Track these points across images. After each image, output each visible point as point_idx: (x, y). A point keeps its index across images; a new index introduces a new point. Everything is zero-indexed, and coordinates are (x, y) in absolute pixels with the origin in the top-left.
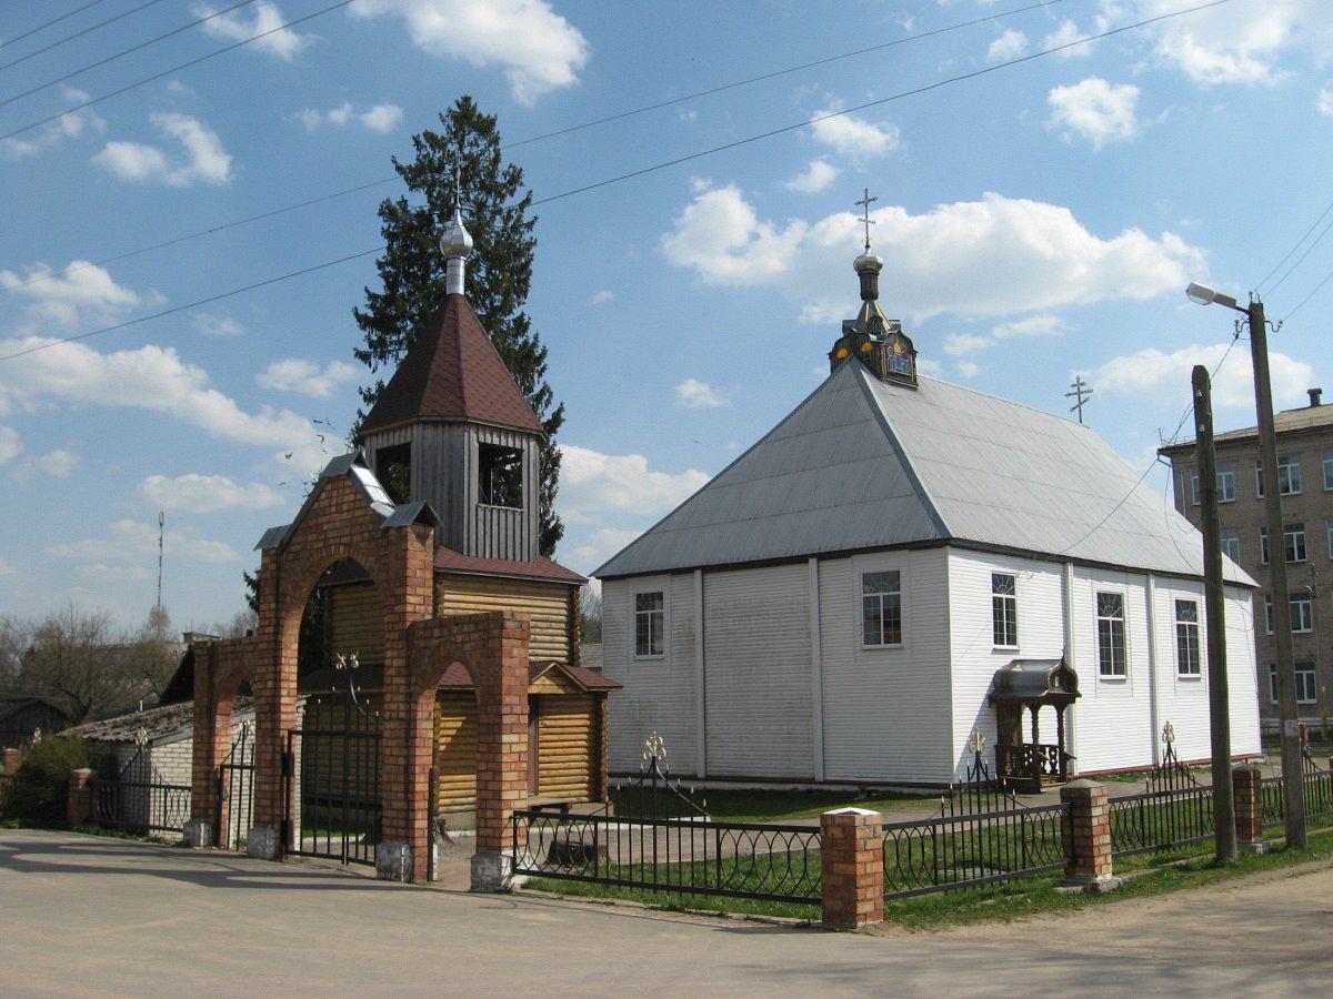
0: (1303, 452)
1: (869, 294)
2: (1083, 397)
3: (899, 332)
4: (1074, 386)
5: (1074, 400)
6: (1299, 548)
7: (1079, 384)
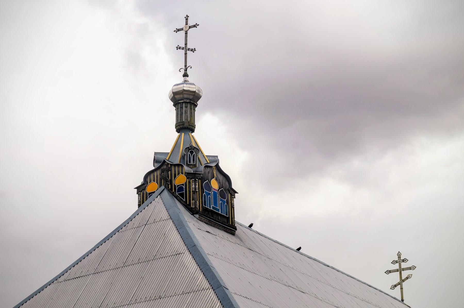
2: (405, 274)
3: (217, 167)
4: (394, 262)
7: (400, 260)
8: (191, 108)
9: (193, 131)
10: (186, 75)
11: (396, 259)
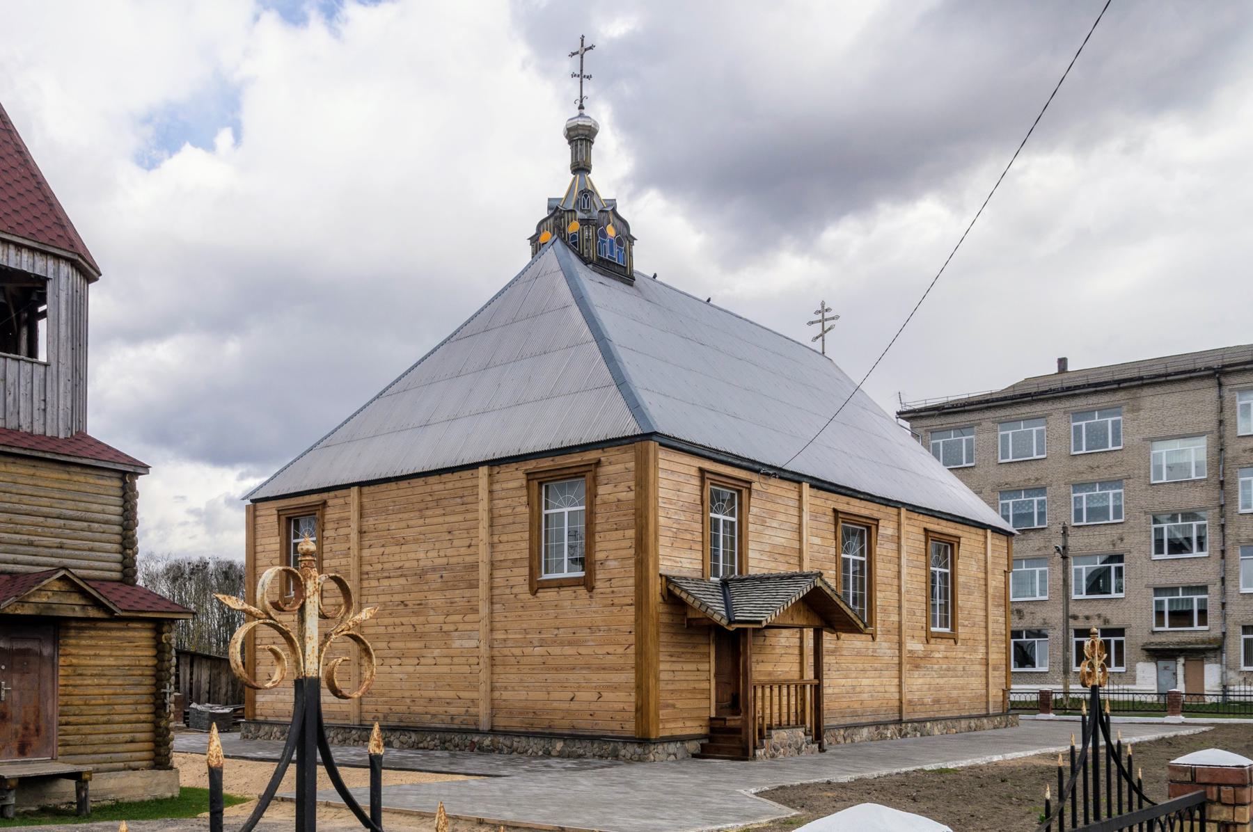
0: (1051, 415)
1: (581, 167)
2: (827, 325)
5: (817, 329)
6: (739, 554)
8: (586, 146)
9: (589, 171)
10: (581, 107)
11: (820, 309)
